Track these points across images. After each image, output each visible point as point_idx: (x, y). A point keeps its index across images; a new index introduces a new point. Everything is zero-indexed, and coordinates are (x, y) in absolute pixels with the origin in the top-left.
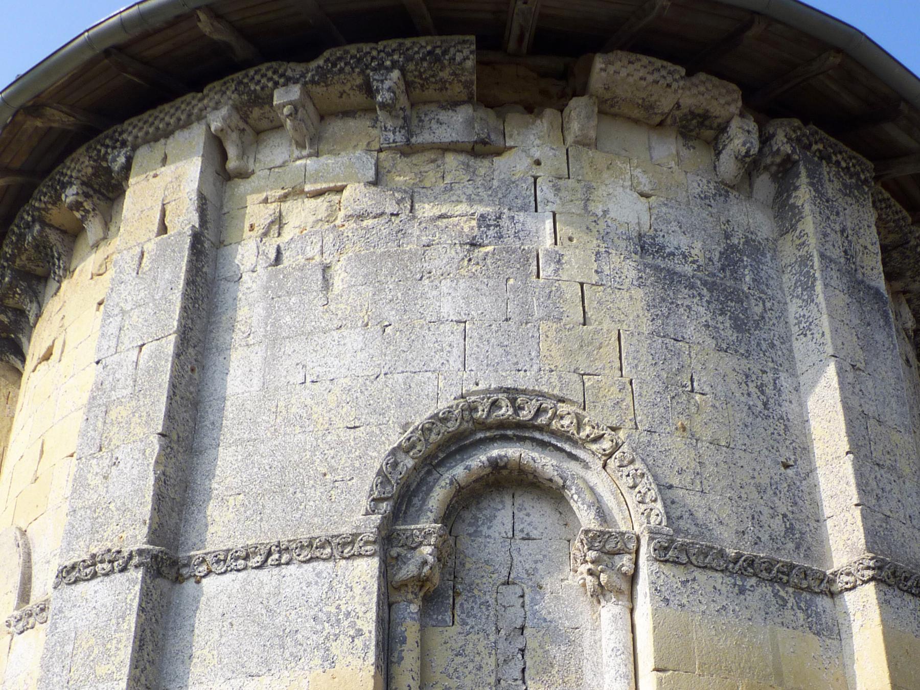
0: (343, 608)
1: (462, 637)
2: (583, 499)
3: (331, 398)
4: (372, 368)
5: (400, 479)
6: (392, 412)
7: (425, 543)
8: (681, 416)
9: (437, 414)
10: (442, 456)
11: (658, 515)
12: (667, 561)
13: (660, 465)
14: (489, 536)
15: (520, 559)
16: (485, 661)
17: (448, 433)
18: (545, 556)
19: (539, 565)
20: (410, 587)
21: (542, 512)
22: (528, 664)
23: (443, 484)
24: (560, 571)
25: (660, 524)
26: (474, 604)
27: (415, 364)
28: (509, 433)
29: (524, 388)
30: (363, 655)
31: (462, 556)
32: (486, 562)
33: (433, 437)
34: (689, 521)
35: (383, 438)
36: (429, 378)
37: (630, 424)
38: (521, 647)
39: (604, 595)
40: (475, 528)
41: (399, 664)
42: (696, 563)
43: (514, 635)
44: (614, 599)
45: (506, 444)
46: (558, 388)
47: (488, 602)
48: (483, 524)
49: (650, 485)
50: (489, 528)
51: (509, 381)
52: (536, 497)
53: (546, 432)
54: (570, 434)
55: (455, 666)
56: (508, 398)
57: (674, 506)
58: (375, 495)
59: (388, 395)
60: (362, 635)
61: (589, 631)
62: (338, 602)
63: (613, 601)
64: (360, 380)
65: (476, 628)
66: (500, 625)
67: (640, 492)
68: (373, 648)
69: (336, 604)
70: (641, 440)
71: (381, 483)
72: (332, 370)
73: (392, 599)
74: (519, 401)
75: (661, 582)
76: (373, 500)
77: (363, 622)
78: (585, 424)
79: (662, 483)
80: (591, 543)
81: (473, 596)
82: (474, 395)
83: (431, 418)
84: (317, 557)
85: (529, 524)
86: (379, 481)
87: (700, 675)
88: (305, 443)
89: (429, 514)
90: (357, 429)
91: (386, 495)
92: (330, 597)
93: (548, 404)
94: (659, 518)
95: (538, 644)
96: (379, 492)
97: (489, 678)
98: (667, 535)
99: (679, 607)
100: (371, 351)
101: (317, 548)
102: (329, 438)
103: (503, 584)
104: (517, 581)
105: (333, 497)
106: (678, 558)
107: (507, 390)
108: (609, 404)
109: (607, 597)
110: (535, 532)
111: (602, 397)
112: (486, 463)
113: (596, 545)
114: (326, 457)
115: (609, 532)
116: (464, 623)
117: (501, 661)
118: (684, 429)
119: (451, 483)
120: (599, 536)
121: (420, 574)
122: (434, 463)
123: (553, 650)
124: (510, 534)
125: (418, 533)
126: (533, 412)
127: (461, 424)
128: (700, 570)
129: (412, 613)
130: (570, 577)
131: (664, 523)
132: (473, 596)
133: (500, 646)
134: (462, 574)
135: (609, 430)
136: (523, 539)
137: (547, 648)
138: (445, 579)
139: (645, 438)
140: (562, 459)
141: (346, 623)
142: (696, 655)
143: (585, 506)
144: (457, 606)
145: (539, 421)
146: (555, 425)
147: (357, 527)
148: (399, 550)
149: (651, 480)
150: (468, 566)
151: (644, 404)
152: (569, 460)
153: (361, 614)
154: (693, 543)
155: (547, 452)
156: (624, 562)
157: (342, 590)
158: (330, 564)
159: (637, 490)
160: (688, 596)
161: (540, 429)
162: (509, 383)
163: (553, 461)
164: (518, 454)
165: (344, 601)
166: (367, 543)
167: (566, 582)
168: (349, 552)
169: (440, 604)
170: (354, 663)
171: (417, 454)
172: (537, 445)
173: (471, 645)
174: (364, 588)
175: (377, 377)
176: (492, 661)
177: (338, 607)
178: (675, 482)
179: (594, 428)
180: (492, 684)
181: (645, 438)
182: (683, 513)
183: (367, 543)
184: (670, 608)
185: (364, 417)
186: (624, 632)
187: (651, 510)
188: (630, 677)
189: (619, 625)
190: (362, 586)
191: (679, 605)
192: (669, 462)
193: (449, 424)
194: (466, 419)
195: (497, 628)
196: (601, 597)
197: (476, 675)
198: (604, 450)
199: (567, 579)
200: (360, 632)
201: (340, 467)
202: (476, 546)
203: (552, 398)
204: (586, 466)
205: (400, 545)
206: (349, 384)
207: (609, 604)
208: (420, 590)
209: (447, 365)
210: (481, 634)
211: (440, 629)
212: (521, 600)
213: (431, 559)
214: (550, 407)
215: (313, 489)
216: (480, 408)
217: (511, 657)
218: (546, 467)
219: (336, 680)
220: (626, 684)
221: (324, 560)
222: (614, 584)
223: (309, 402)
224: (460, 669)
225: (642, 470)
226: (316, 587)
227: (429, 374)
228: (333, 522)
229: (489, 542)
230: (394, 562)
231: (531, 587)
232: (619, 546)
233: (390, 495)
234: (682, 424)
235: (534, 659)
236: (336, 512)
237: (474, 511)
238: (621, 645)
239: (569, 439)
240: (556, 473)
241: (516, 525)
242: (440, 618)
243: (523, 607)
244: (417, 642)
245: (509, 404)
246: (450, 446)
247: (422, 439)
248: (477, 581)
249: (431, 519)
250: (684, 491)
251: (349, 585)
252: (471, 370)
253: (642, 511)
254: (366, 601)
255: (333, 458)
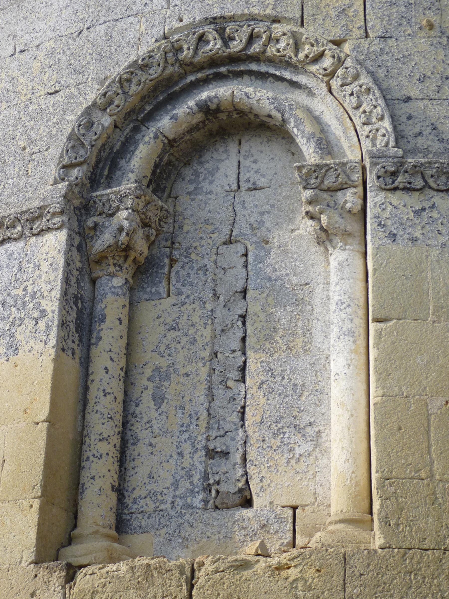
0: (30, 289)
1: (176, 309)
2: (303, 132)
3: (36, 65)
4: (76, 24)
5: (95, 141)
6: (92, 68)
7: (121, 207)
8: (427, 12)
9: (136, 62)
10: (148, 108)
11: (384, 135)
12: (396, 189)
13: (396, 76)
14: (211, 192)
15: (244, 212)
16: (200, 333)
17: (151, 81)
18: (273, 206)
19: (266, 217)
20: (110, 258)
21: (272, 156)
22: (248, 332)
23: (147, 139)
24: (291, 220)
25: (386, 145)
26: (190, 271)
27: (117, 11)
28: (223, 70)
29: (232, 14)
30: (45, 338)
31: (181, 218)
32: (206, 222)
33: (134, 89)
34: (431, 137)
35: (81, 99)
36: (131, 23)
37: (357, 33)
38: (241, 312)
39: (331, 241)
40: (195, 185)
41: (97, 345)
42: (434, 186)
43: (234, 300)
44: (340, 244)
45: (222, 84)
46: (271, 7)
47: (206, 266)
48: (204, 179)
49: (377, 101)
50: (211, 183)
51: (216, 10)
52: (265, 140)
53: (264, 61)
54: (287, 59)
55: (167, 343)
56: (215, 30)
57: (411, 122)
58: (66, 161)
59: (89, 51)
60: (45, 316)
61: (321, 286)
62: (25, 283)
63: (339, 245)
64: (64, 40)
65: (192, 297)
66: (219, 290)
67: (365, 112)
68: (55, 329)
69: (23, 286)
70: (371, 50)
71: (73, 147)
72: (39, 35)
73: (94, 275)
74: (228, 30)
75: (386, 214)
76: (64, 167)
77: (47, 302)
78: (304, 44)
79: (396, 97)
80: (306, 181)
81: (190, 261)
82: (178, 33)
83: (129, 66)
84: (9, 238)
85: (256, 172)
86: (70, 146)
87: (434, 322)
88: (9, 118)
89: (130, 175)
90: (58, 94)
91: (77, 161)
92: (19, 279)
93: (260, 28)
94: (386, 139)
95: (260, 308)
96: (70, 158)
97: (203, 352)
98: (394, 157)
99: (410, 243)
100: (76, 6)
101: (8, 228)
102: (31, 108)
103: (225, 243)
104: (240, 239)
105: (30, 171)
106: (410, 183)
107: (213, 20)
108: (332, 13)
109: (334, 242)
110: (263, 180)
111: (324, 8)
112: (195, 108)
113: (313, 181)
114: (26, 129)
115: (327, 165)
116: (179, 293)
117: (218, 333)
118: (431, 26)
119: (156, 137)
120: (315, 171)
121: (116, 243)
122: (140, 118)
123: (279, 313)
124: (234, 187)
125: (114, 197)
126: (244, 41)
127: (164, 69)
128: (441, 194)
129: (115, 288)
130: (302, 226)
131: (392, 143)
132: (190, 261)
133: (218, 314)
134: (179, 239)
135: (330, 45)
136: (249, 189)
137: (271, 310)
138: (162, 246)
139: (377, 46)
140: (284, 90)
141: (31, 305)
142: (430, 297)
143: (305, 139)
144: (173, 275)
145: (252, 50)
146: (271, 51)
147: (45, 199)
148: (96, 219)
149: (378, 95)
150: (186, 228)
151: (378, 5)
152: (292, 89)
153: (46, 294)
154: (430, 163)
155: (267, 84)
156: (348, 198)
157: (30, 269)
158: (21, 244)
159: (361, 110)
160: (423, 228)
161: (256, 59)
162: (216, 12)
163: (269, 93)
164: (229, 92)
165: (31, 282)
166: (54, 215)
167: (297, 233)
168: (37, 228)
169: (155, 274)
170: (36, 347)
171: (115, 110)
172: (256, 78)
173: (185, 317)
174: (51, 265)
175: (80, 33)
176: (207, 332)
177: (25, 289)
178: (415, 92)
179: (313, 45)
180: (207, 358)
181: (377, 46)
182: (424, 128)
183: (54, 215)
184: (398, 244)
185: (64, 79)
186: (351, 280)
187: (377, 130)
188: (357, 334)
189: (345, 273)
190: (49, 262)
191: (409, 240)
192: (407, 70)
193: (151, 71)
194: (170, 61)
195: (215, 294)
196: (327, 243)
197: (189, 349)
198: (325, 69)
199: (299, 229)
200: (43, 313)
201: (38, 138)
202: (195, 205)
203: (265, 19)
204: (311, 94)
205: (98, 213)
206: (53, 46)
207: (337, 250)
208: (125, 261)
209: (150, 5)
210: (197, 303)
211: (154, 303)
212: (244, 259)
213: (126, 224)
214: (262, 30)
215: (12, 166)
216: (185, 46)
217: (229, 326)
218: (261, 102)
219: (18, 368)
220: (351, 343)
221: (16, 240)
222: (337, 226)
223: (16, 74)
224: (173, 345)
225: (367, 84)
226: (7, 270)
227: (132, 18)
228: (27, 197)
229: (210, 199)
230: (92, 233)
231: (256, 242)
232: (340, 179)
233: (82, 159)
234: (428, 21)
235: (256, 325)
236: (31, 186)
237: (195, 164)
238: (346, 296)
239: (289, 65)
240: (272, 107)
241: (241, 174)
242: (153, 290)
243: (246, 267)
244: (120, 319)
245: (217, 36)
246: (158, 96)
247: (120, 91)
248: (195, 244)
249: (132, 180)
250: (426, 102)
251: (37, 264)
252: (176, 5)
253: (366, 133)
254: (52, 278)
255: (32, 129)
